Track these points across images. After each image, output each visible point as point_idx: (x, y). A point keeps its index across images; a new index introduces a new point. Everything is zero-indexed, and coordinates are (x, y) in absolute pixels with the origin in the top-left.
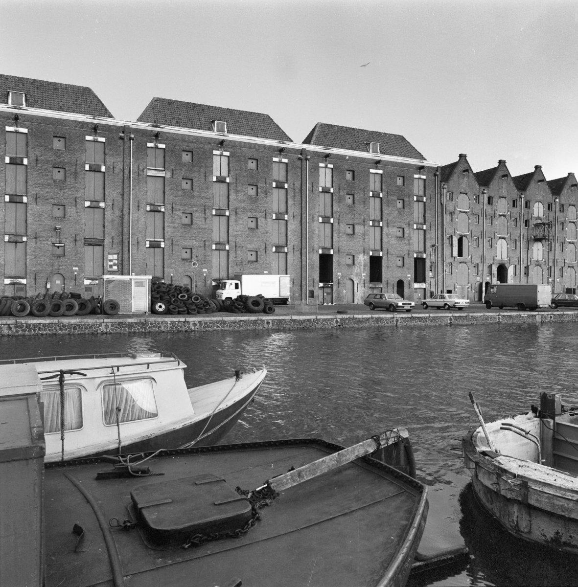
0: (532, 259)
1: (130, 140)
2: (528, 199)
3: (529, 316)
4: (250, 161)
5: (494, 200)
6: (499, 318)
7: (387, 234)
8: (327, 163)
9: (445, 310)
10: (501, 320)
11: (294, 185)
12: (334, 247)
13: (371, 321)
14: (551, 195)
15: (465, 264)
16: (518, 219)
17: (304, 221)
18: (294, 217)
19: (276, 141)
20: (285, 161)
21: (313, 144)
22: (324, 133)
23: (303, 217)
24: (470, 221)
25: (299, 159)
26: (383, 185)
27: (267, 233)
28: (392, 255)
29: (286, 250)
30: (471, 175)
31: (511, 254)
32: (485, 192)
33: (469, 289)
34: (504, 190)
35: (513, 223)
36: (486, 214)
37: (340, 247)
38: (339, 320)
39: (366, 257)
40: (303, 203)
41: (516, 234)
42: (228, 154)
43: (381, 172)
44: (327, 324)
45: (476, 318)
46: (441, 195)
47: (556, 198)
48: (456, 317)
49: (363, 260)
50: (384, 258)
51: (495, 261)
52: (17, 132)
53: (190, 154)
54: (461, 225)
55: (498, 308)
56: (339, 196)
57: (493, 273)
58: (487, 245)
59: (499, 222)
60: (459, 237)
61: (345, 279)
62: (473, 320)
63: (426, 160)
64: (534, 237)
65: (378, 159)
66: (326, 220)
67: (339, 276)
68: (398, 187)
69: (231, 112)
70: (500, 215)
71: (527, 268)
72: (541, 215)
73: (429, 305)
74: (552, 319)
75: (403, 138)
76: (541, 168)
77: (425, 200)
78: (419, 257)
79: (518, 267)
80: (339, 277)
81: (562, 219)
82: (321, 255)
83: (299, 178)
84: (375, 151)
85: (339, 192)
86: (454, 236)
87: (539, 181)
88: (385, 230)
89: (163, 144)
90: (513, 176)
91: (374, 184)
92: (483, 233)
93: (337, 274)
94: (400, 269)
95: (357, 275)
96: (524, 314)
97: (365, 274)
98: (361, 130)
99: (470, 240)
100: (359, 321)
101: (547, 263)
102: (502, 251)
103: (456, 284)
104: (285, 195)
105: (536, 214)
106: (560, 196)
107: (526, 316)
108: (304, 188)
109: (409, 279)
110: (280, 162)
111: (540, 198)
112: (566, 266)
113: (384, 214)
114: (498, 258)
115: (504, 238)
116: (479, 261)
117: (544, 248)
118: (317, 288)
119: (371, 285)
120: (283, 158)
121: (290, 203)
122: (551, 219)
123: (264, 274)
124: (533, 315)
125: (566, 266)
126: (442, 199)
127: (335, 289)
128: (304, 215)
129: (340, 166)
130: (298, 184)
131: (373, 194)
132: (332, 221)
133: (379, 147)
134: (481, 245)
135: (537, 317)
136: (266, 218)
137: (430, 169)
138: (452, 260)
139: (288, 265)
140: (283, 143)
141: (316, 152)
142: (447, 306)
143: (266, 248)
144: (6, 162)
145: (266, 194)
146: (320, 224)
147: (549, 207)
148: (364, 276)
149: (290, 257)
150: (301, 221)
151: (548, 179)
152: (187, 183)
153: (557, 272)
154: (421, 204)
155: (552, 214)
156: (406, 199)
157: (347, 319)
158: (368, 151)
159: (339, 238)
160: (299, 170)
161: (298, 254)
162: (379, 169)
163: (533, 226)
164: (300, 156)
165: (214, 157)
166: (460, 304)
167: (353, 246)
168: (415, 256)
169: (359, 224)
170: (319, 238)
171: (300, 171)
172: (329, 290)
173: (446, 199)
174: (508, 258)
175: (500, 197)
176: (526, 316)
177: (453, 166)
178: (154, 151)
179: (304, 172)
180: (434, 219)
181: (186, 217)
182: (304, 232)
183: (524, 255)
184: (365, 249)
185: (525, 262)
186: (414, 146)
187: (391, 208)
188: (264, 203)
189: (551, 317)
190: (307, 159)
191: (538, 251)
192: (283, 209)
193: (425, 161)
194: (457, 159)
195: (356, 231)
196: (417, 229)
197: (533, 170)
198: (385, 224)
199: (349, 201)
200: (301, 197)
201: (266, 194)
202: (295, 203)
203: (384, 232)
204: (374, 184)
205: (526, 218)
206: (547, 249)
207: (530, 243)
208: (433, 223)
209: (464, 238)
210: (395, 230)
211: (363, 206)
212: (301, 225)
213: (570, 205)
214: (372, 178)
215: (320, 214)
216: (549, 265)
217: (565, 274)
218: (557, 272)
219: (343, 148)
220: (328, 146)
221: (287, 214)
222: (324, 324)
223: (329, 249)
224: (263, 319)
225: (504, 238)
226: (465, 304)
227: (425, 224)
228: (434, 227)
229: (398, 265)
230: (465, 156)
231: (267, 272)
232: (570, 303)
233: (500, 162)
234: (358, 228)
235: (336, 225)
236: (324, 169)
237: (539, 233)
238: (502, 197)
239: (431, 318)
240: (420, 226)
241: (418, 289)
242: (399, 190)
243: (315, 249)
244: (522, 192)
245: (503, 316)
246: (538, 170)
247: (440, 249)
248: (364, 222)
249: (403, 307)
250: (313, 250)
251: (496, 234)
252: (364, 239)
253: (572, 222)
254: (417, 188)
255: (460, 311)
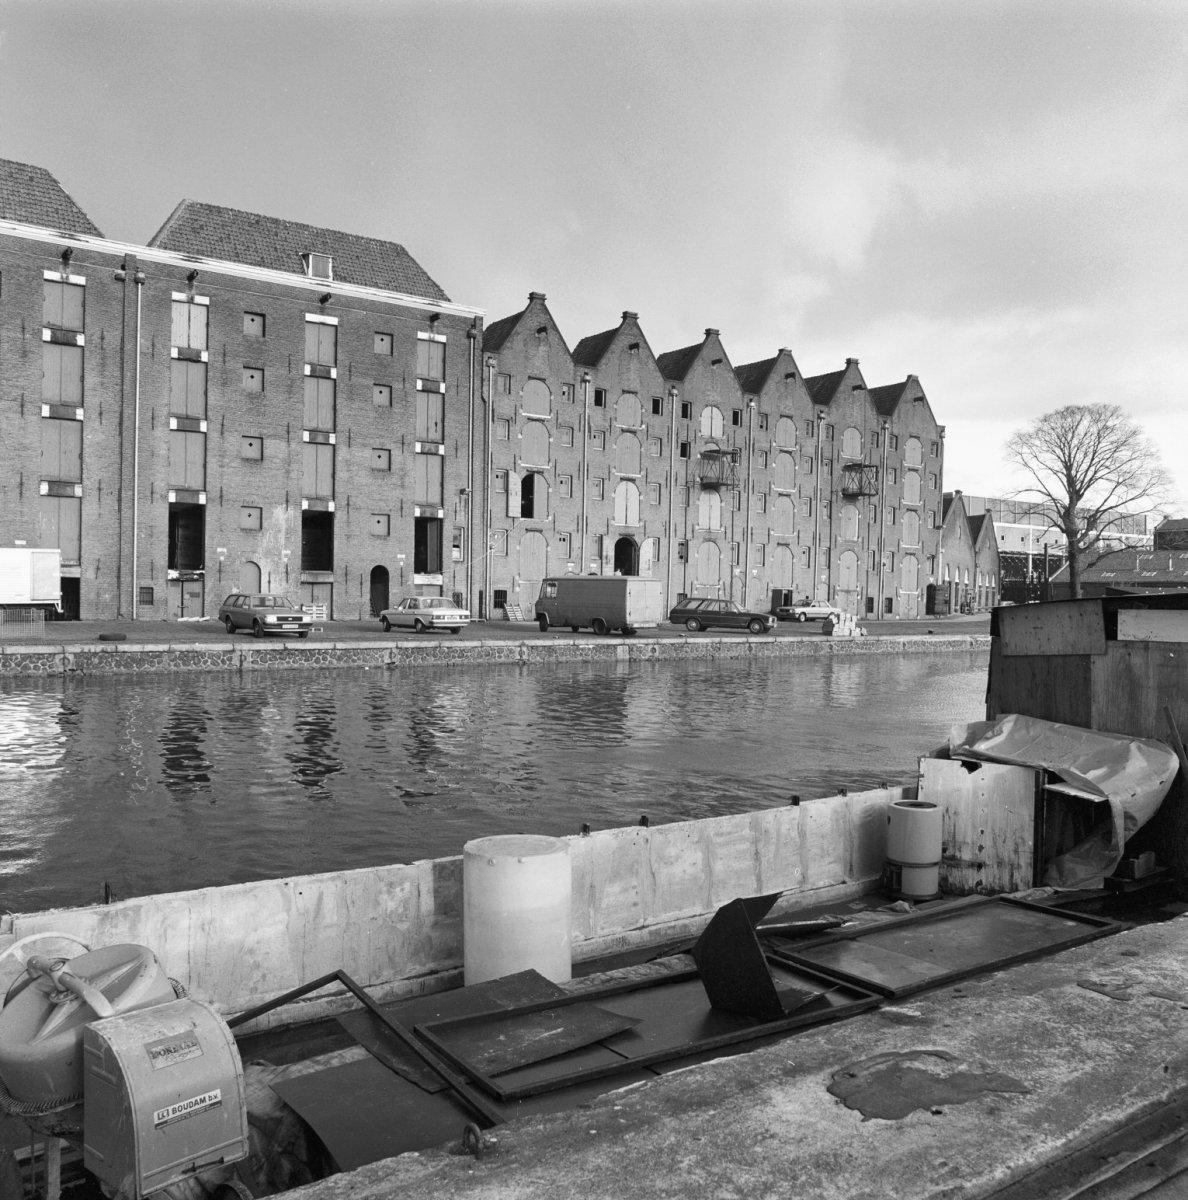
0: (697, 527)
1: (137, 283)
2: (688, 398)
3: (598, 648)
4: (377, 338)
5: (695, 410)
6: (654, 650)
7: (348, 463)
8: (194, 291)
9: (417, 633)
10: (525, 657)
11: (102, 338)
12: (208, 487)
13: (165, 658)
14: (739, 393)
15: (538, 534)
16: (665, 440)
17: (126, 424)
18: (101, 414)
19: (53, 231)
20: (75, 279)
21: (159, 247)
22: (200, 227)
23: (125, 416)
24: (551, 440)
25: (118, 279)
26: (339, 351)
27: (26, 448)
28: (358, 509)
29: (78, 491)
30: (799, 383)
31: (647, 515)
32: (588, 378)
33: (721, 592)
34: (633, 376)
35: (655, 449)
36: (590, 428)
37: (225, 489)
38: (71, 657)
39: (291, 511)
40: (127, 381)
41: (659, 474)
42: (206, 300)
43: (334, 321)
44: (36, 668)
45: (462, 652)
46: (482, 380)
47: (751, 400)
48: (406, 649)
49: (285, 522)
50: (209, 506)
51: (611, 529)
52: (432, 341)
53: (258, 320)
54: (532, 450)
55: (570, 629)
56: (224, 372)
57: (604, 554)
58: (593, 492)
59: (781, 464)
60: (524, 474)
61: (238, 562)
62: (454, 657)
63: (449, 301)
64: (702, 479)
65: (325, 290)
66: (188, 425)
67: (222, 554)
68: (378, 356)
69: (340, 237)
70: (623, 431)
71: (684, 545)
72: (718, 433)
73: (391, 622)
74: (657, 654)
75: (403, 249)
76: (637, 318)
77: (443, 390)
78: (428, 515)
79: (664, 542)
80: (222, 558)
81: (765, 446)
82: (305, 513)
83: (117, 324)
84: (320, 273)
85: (224, 362)
86: (511, 473)
87: (714, 362)
88: (343, 453)
89: (335, 316)
90: (805, 376)
91: (316, 347)
92: (582, 469)
93: (216, 548)
94: (379, 541)
95: (268, 553)
96: (587, 643)
97: (289, 552)
98: (297, 224)
99: (551, 480)
100: (133, 660)
101: (729, 535)
102: (626, 509)
103: (517, 578)
104: (331, 391)
105: (705, 432)
106: (759, 396)
107: (591, 647)
108: (128, 347)
109: (402, 563)
110: (64, 282)
111: (714, 397)
112: (773, 544)
113: (340, 416)
114: (619, 522)
115: (632, 480)
116: (572, 527)
117: (723, 504)
118: (162, 581)
119: (304, 577)
120: (73, 273)
121: (91, 380)
122: (740, 443)
123: (14, 546)
124: (608, 646)
125: (773, 544)
126: (485, 389)
127: (209, 584)
128: (127, 412)
129: (226, 302)
130: (113, 338)
131: (313, 370)
132: (203, 427)
133: (330, 265)
134: (577, 494)
135: (620, 649)
136: (22, 413)
137: (454, 321)
138: (507, 524)
139: (83, 526)
140: (71, 237)
141: (165, 265)
142: (420, 626)
143: (21, 484)
144: (44, 339)
145: (24, 354)
146: (173, 433)
147: (736, 418)
148: (286, 556)
149: (90, 509)
150: (121, 424)
151: (871, 384)
152: (381, 392)
153: (753, 556)
154: (435, 399)
155: (741, 433)
156: (397, 386)
157: (95, 654)
158: (303, 272)
159: (221, 466)
160: (116, 307)
161: (110, 502)
162: (328, 315)
163: (699, 456)
164: (120, 271)
165: (175, 306)
166: (446, 620)
167: (259, 487)
168: (417, 513)
169: (274, 436)
170: (172, 469)
171: (120, 308)
172: (196, 587)
173: (496, 389)
174: (642, 524)
175: (624, 392)
176: (591, 647)
177: (608, 337)
178: (427, 347)
179: (129, 311)
180: (465, 433)
181: (251, 445)
182: (127, 452)
183: (677, 518)
184: (290, 494)
185: (680, 533)
186: (426, 270)
187: (355, 405)
188: (19, 377)
189: (654, 650)
190: (137, 281)
191: (710, 510)
192: (72, 394)
193: (444, 304)
194: (522, 304)
195: (267, 452)
196: (422, 453)
197: (700, 339)
198: (344, 437)
199: (254, 385)
200: (122, 369)
201: (24, 354)
202: (105, 381)
203: (339, 458)
204: (316, 347)
205: (683, 438)
206: (729, 506)
207: (691, 490)
208: (462, 441)
209: (537, 477)
210: (368, 453)
211: (286, 395)
212: (121, 434)
213: (781, 416)
214: (310, 334)
215: (174, 410)
216: (735, 538)
217: (769, 560)
218: (753, 556)
219: (239, 261)
220: (195, 253)
221: (82, 406)
222: (26, 667)
223: (197, 492)
224: (898, 640)
225: (632, 480)
226: (458, 620)
227: (443, 444)
228: (465, 450)
229: (376, 532)
230: (635, 317)
231: (24, 543)
232: (724, 620)
233: (708, 332)
234: (274, 447)
235: (214, 436)
236: (186, 305)
237: (712, 472)
238: (629, 392)
239: (338, 653)
240: (432, 447)
241: (424, 588)
242: (381, 364)
243: (157, 489)
244: (823, 408)
245: (532, 647)
246: (712, 336)
247: (478, 498)
248: (288, 432)
249: (280, 626)
250: (152, 493)
251: (613, 471)
252: (288, 472)
253: (786, 452)
254: (426, 364)
255: (455, 636)
